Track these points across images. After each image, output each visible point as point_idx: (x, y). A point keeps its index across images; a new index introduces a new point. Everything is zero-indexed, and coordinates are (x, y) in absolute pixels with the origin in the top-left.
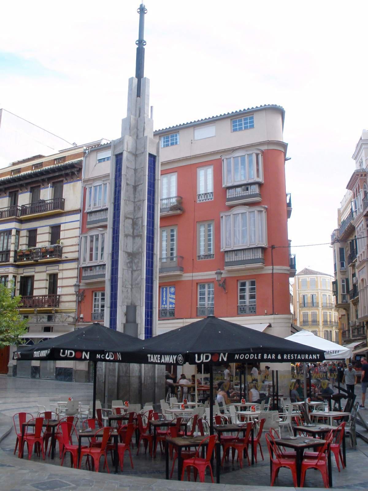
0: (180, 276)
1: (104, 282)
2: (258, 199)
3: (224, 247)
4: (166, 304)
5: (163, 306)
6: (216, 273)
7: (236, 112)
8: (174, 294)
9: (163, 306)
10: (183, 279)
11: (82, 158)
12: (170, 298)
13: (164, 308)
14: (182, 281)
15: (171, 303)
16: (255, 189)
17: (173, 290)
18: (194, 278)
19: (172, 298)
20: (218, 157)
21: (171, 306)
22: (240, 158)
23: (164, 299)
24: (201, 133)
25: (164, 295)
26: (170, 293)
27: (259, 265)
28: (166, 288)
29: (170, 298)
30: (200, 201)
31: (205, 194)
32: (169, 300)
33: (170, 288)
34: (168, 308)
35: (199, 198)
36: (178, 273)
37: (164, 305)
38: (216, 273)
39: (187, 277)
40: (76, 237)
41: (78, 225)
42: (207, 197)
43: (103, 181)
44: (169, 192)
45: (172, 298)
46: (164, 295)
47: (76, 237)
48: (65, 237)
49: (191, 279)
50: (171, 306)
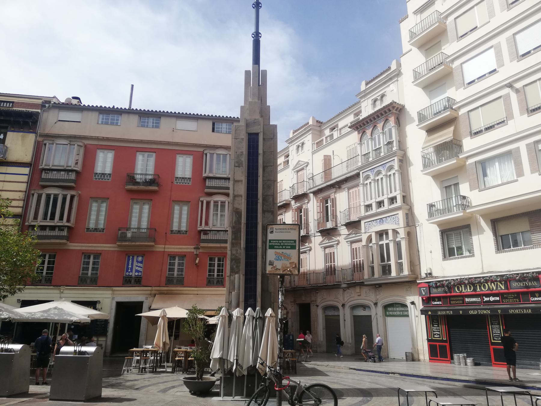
0: (152, 246)
1: (226, 248)
2: (73, 184)
3: (30, 221)
4: (132, 271)
5: (128, 274)
6: (194, 248)
7: (219, 116)
8: (141, 262)
9: (128, 274)
10: (158, 250)
11: (39, 111)
12: (137, 266)
13: (129, 275)
14: (153, 251)
15: (137, 271)
16: (73, 176)
17: (140, 259)
18: (166, 250)
19: (139, 267)
20: (201, 150)
21: (137, 274)
22: (222, 156)
23: (130, 266)
24: (182, 124)
25: (130, 263)
26: (137, 262)
27: (64, 241)
28: (133, 257)
29: (137, 266)
30: (96, 179)
31: (103, 174)
32: (135, 268)
33: (138, 256)
34: (133, 276)
35: (95, 176)
36: (153, 244)
37: (129, 272)
38: (194, 248)
39: (160, 248)
40: (20, 191)
41: (25, 179)
42: (104, 177)
43: (70, 141)
44: (104, 167)
45: (139, 267)
46: (130, 263)
47: (20, 191)
48: (4, 189)
49: (163, 250)
50: (137, 274)
